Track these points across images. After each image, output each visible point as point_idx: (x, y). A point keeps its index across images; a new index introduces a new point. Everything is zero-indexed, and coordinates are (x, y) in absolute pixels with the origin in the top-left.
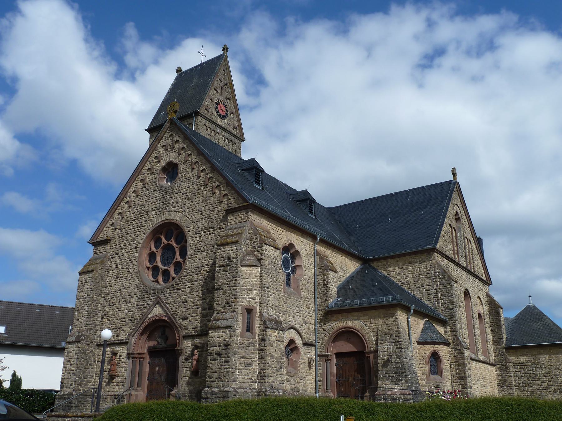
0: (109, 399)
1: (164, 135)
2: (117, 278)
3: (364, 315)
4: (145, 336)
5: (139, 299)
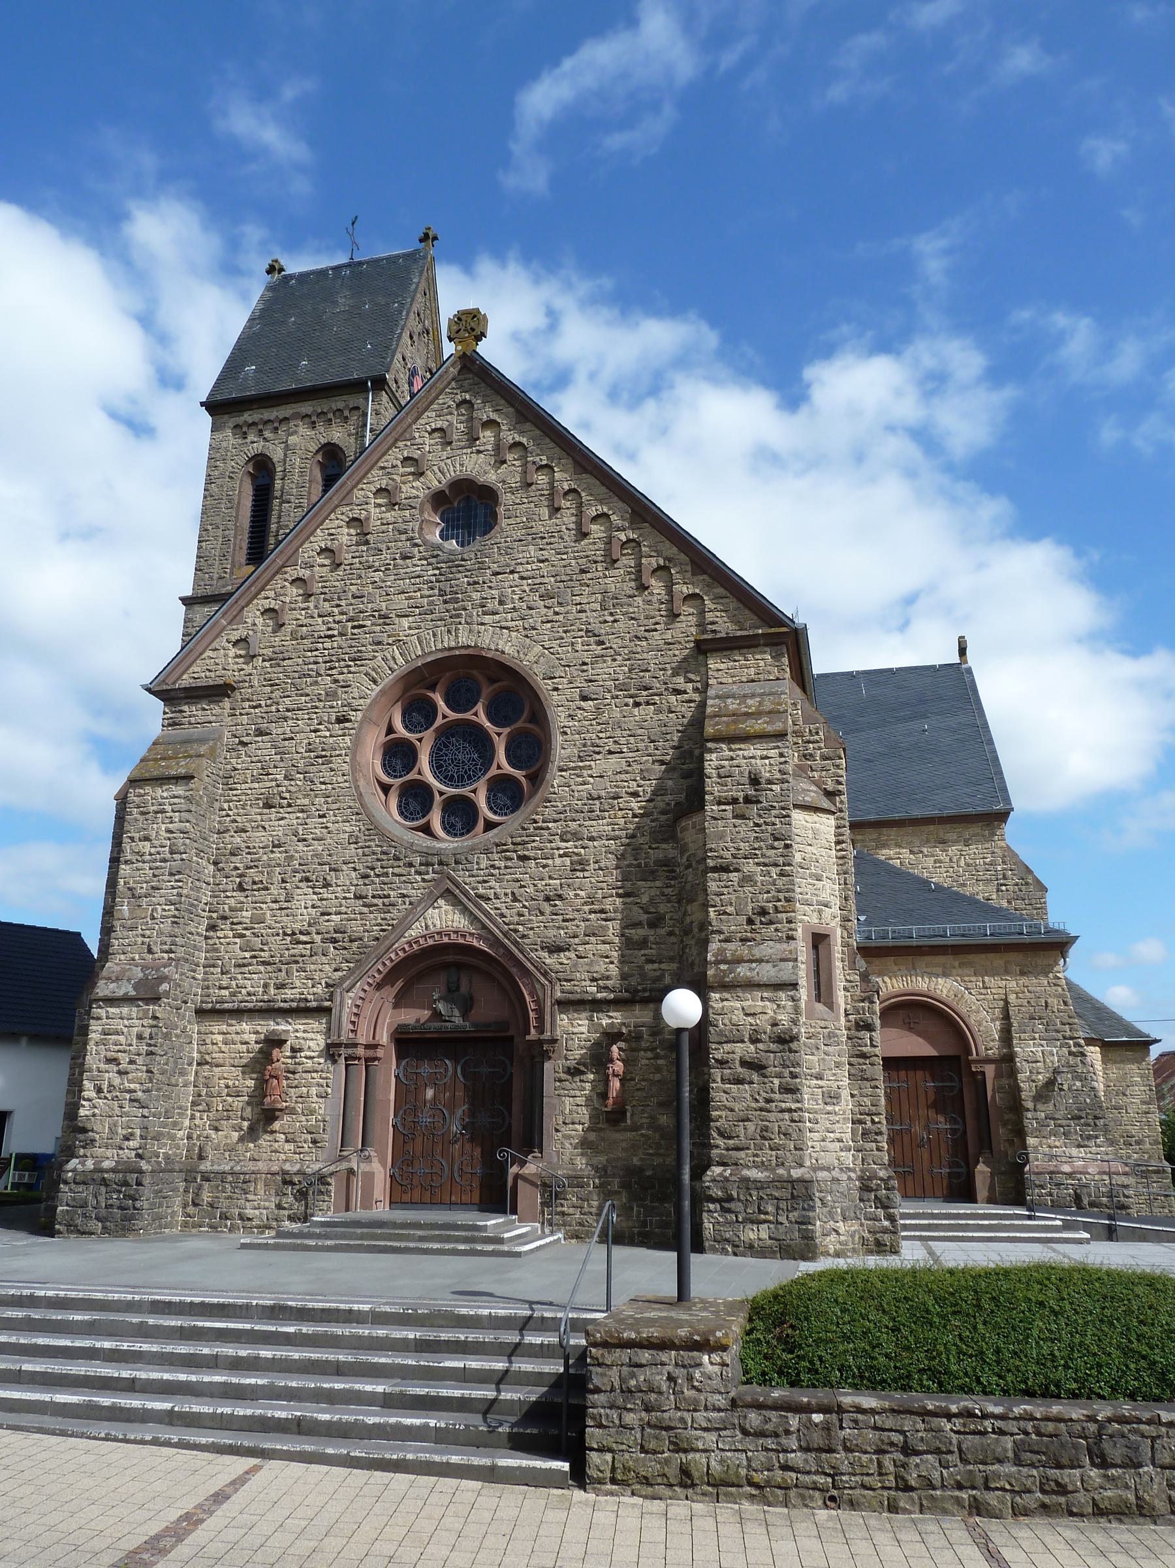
0: (260, 1186)
1: (437, 398)
2: (268, 806)
3: (961, 965)
4: (390, 992)
5: (366, 876)
